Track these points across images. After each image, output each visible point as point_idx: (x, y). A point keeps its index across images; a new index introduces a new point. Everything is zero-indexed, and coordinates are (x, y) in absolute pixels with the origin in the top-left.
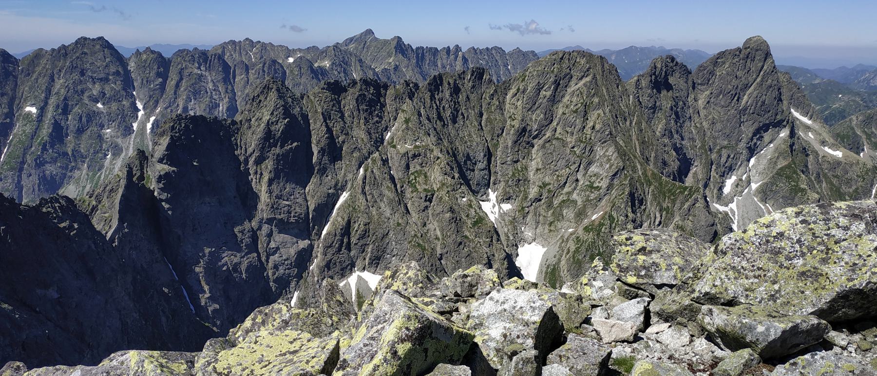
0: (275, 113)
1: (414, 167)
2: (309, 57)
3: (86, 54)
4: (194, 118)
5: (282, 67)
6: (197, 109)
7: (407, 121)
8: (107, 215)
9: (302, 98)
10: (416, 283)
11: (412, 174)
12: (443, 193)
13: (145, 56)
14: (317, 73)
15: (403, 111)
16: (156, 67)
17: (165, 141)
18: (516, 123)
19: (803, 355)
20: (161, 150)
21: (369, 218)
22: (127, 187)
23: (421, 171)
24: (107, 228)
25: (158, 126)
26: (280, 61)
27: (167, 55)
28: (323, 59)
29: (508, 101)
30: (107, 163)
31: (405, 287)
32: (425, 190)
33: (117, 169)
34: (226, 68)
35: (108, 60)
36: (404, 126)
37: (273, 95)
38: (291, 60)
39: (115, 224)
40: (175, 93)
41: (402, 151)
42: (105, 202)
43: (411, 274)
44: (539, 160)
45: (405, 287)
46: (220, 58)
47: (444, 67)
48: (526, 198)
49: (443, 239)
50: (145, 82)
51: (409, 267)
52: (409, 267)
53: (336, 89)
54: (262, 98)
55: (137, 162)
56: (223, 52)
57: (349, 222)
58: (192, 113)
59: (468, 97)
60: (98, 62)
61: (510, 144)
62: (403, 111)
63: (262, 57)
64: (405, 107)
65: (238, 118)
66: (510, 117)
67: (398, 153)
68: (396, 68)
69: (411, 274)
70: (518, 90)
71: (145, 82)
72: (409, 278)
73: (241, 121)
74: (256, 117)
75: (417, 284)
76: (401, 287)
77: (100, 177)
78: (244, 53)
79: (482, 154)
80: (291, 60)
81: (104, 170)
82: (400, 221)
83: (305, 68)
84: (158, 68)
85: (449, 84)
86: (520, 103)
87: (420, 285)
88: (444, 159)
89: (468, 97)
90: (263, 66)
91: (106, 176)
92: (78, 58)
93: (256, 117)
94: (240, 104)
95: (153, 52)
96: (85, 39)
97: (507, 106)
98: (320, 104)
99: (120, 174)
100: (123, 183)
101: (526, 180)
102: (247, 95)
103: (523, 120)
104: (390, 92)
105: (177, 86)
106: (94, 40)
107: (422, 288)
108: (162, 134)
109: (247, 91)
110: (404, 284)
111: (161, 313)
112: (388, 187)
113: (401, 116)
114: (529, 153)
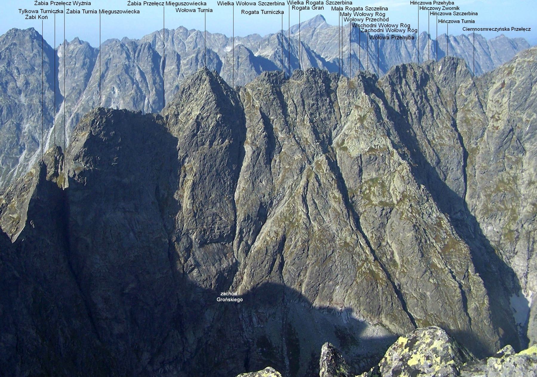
0: (206, 108)
1: (368, 174)
2: (249, 46)
3: (15, 44)
4: (117, 112)
5: (218, 57)
6: (120, 103)
7: (362, 119)
8: (15, 216)
9: (239, 90)
10: (445, 358)
11: (366, 182)
12: (406, 206)
13: (72, 47)
14: (258, 63)
15: (357, 107)
16: (82, 58)
17: (83, 137)
18: (501, 125)
19: (477, 270)
20: (78, 146)
21: (309, 234)
22: (39, 187)
23: (377, 179)
24: (13, 230)
25: (77, 120)
26: (216, 51)
27: (95, 45)
28: (264, 48)
29: (490, 98)
30: (22, 158)
31: (429, 362)
32: (381, 203)
33: (30, 166)
34: (155, 57)
35: (35, 51)
36: (358, 125)
37: (206, 86)
38: (229, 49)
39: (23, 226)
40: (99, 85)
41: (355, 153)
42: (15, 202)
43: (437, 344)
44: (532, 170)
45: (429, 362)
46: (151, 47)
47: (409, 55)
48: (515, 219)
49: (402, 266)
50: (69, 73)
51: (434, 337)
52: (434, 337)
53: (277, 82)
54: (193, 90)
55: (51, 159)
56: (154, 42)
57: (284, 239)
58: (113, 106)
59: (439, 91)
60: (29, 51)
61: (493, 149)
62: (357, 107)
63: (196, 46)
64: (359, 102)
65: (164, 113)
66: (493, 117)
67: (349, 156)
68: (352, 56)
69: (437, 344)
70: (503, 84)
71: (69, 73)
72: (435, 351)
73: (167, 117)
74: (185, 112)
75: (447, 361)
76: (423, 361)
77: (12, 174)
78: (176, 42)
79: (456, 161)
80: (229, 49)
81: (17, 167)
82: (348, 240)
83: (244, 56)
84: (85, 59)
85: (415, 75)
86: (505, 100)
87: (452, 362)
88: (405, 167)
89: (439, 91)
90: (197, 55)
91: (19, 174)
92: (7, 49)
93: (185, 112)
94: (169, 98)
95: (80, 42)
96: (17, 30)
97: (490, 104)
98: (258, 99)
99: (34, 171)
100: (35, 181)
101: (516, 196)
102: (177, 87)
103: (509, 121)
104: (342, 84)
105: (102, 77)
106: (24, 31)
107: (454, 366)
108: (82, 129)
109: (176, 83)
110: (428, 358)
111: (60, 332)
112: (335, 197)
113: (355, 114)
114: (519, 161)
